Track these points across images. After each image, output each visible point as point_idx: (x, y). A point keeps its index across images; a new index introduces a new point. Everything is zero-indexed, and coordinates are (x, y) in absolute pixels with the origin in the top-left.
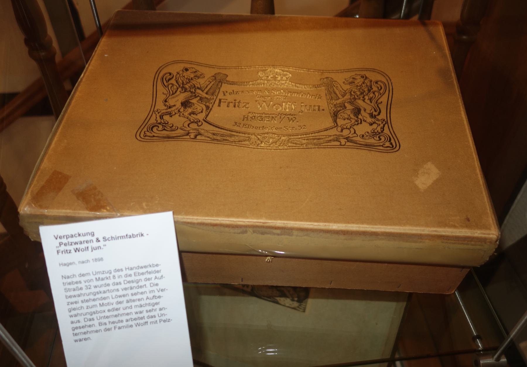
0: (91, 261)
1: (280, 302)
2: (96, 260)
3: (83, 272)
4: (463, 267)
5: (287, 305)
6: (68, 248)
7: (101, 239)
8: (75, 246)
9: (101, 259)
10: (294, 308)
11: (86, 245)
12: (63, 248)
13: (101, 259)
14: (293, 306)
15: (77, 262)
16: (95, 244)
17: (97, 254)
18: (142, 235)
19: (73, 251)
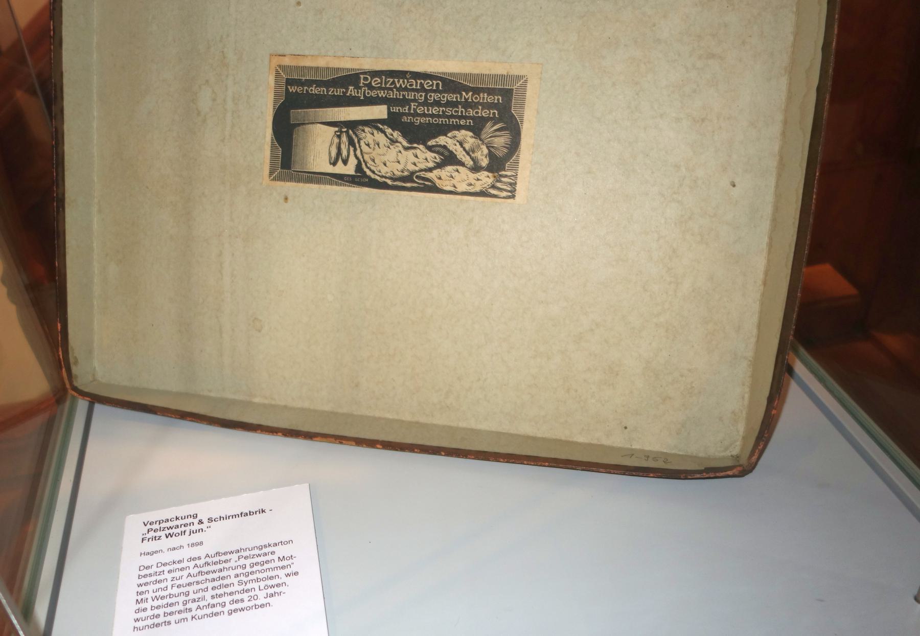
0: (186, 546)
1: (439, 183)
2: (193, 545)
3: (177, 559)
4: (783, 371)
5: (462, 187)
6: (158, 534)
7: (205, 521)
8: (167, 532)
9: (201, 543)
10: (482, 194)
11: (183, 529)
12: (152, 534)
13: (201, 543)
14: (478, 189)
15: (165, 550)
16: (197, 527)
17: (196, 538)
18: (263, 511)
19: (164, 537)
